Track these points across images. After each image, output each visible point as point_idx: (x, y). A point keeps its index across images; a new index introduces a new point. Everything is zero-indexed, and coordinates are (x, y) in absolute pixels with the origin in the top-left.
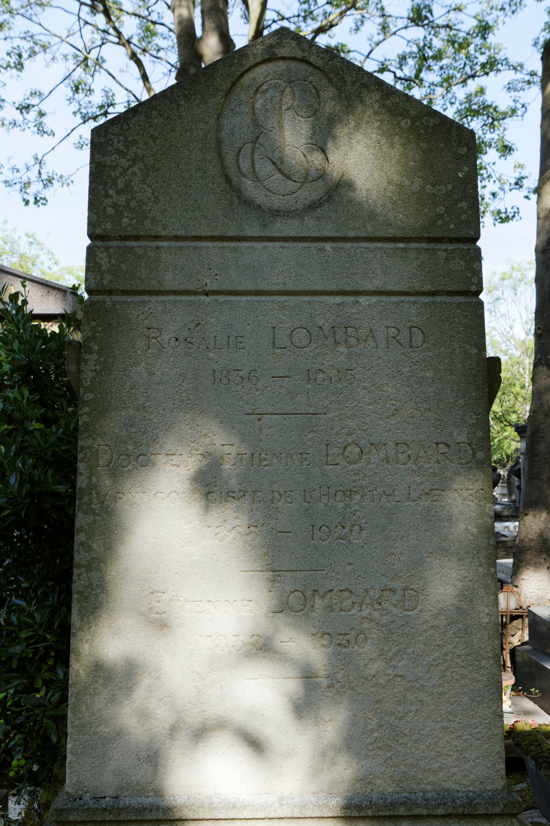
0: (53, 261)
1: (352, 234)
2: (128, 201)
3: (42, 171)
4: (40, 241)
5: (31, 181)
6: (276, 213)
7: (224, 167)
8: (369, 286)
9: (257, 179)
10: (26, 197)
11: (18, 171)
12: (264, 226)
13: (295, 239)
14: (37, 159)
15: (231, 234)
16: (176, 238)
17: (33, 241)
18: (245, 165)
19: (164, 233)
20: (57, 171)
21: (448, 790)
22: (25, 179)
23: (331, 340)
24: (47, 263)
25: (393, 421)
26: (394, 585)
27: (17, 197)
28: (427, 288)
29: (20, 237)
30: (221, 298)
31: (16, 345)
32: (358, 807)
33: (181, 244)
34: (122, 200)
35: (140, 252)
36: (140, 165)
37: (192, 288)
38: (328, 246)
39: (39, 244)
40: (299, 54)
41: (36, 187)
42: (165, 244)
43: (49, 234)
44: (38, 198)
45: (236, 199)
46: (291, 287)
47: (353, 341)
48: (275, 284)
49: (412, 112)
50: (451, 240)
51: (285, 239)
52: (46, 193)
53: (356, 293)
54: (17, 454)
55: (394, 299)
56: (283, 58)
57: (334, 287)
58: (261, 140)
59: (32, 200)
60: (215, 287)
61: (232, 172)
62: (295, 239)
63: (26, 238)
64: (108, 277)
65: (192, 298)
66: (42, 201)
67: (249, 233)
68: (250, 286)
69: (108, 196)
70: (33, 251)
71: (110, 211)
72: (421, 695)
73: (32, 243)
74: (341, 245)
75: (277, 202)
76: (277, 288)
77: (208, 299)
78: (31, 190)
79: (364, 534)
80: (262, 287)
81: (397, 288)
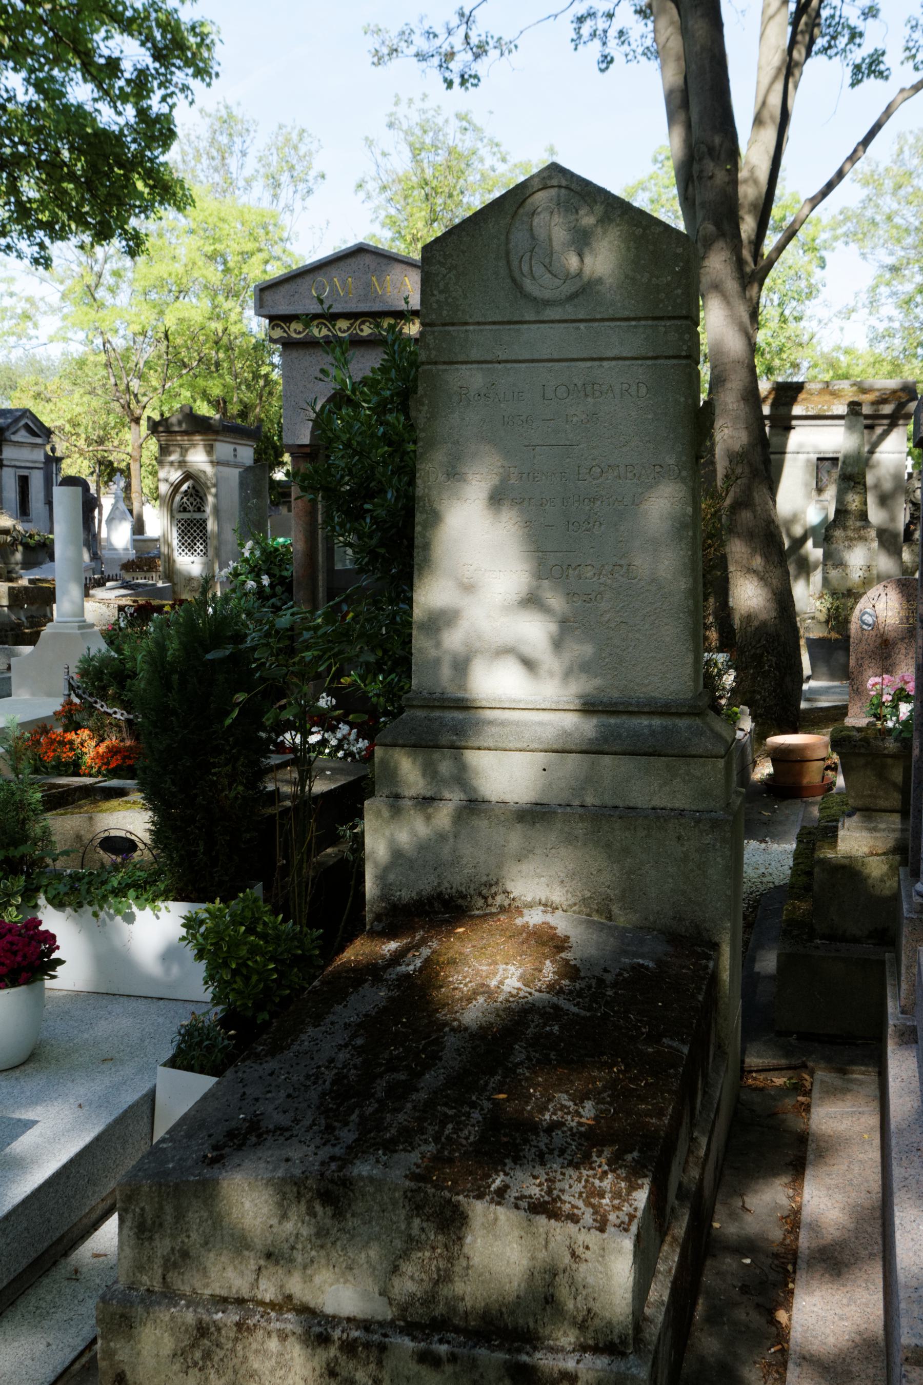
0: (499, 156)
1: (598, 317)
2: (446, 298)
3: (470, 33)
4: (478, 124)
5: (455, 50)
6: (547, 303)
7: (510, 270)
8: (609, 354)
9: (534, 278)
10: (448, 74)
11: (435, 36)
12: (538, 312)
13: (559, 321)
14: (462, 15)
15: (515, 319)
16: (478, 323)
17: (467, 126)
18: (525, 268)
19: (470, 321)
20: (491, 33)
21: (654, 698)
22: (446, 48)
23: (582, 393)
24: (489, 161)
25: (624, 449)
26: (622, 562)
27: (436, 77)
28: (650, 354)
29: (447, 121)
30: (509, 365)
31: (393, 374)
32: (593, 704)
33: (482, 327)
34: (442, 297)
35: (455, 334)
36: (454, 272)
37: (489, 359)
38: (582, 326)
39: (476, 129)
40: (564, 183)
41: (463, 58)
42: (471, 328)
43: (491, 112)
44: (466, 77)
45: (519, 295)
46: (556, 356)
47: (597, 394)
48: (545, 354)
49: (644, 223)
50: (670, 318)
51: (552, 322)
52: (479, 67)
53: (601, 359)
54: (393, 473)
55: (627, 363)
56: (553, 187)
57: (585, 356)
58: (536, 250)
59: (457, 81)
60: (504, 357)
61: (517, 274)
62: (559, 321)
63: (457, 121)
64: (434, 353)
65: (490, 366)
66: (472, 80)
67: (527, 318)
68: (528, 357)
69: (433, 295)
70: (465, 143)
71: (435, 306)
72: (637, 635)
73: (466, 129)
74: (591, 324)
75: (547, 295)
76: (546, 357)
77: (500, 366)
78: (456, 66)
79: (603, 528)
80: (536, 357)
81: (629, 355)
